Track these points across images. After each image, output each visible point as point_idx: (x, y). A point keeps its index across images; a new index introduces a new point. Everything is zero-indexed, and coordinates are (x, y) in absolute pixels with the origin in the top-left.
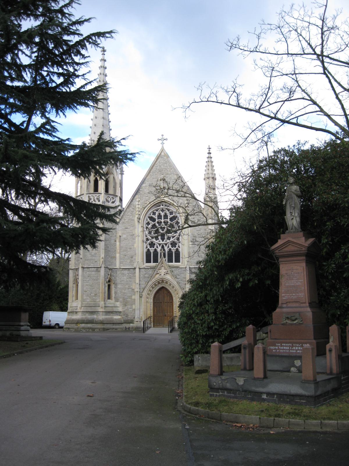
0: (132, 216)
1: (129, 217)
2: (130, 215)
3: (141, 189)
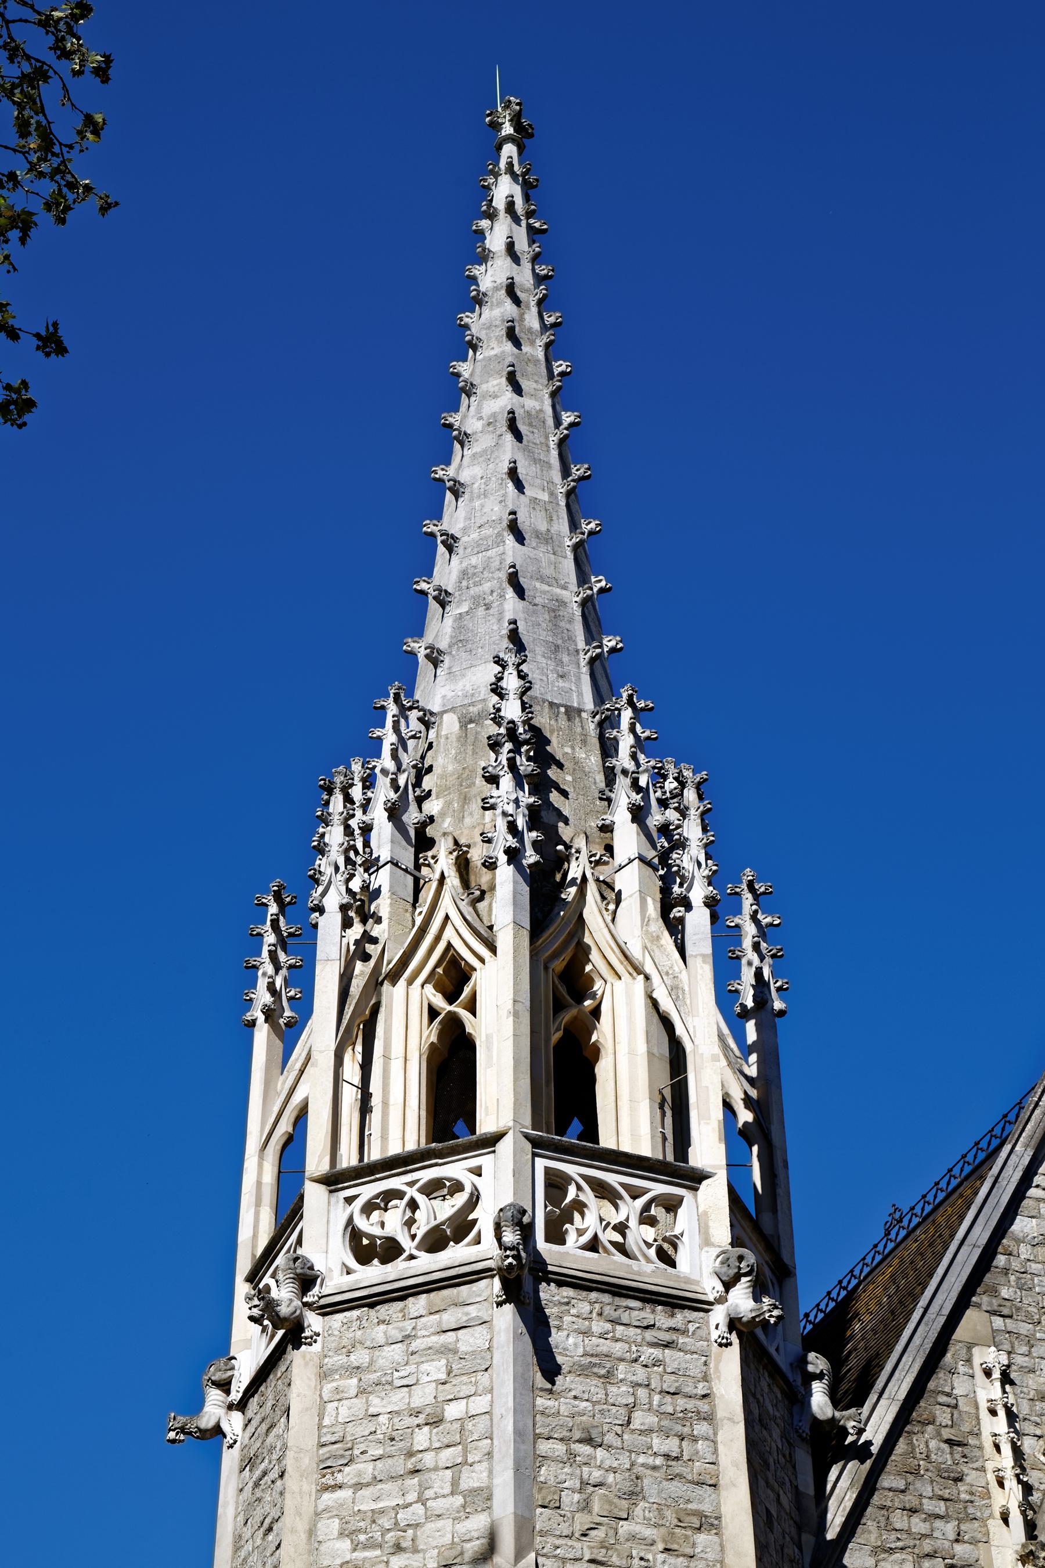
0: (949, 1529)
1: (918, 1525)
2: (929, 1506)
3: (1001, 1260)
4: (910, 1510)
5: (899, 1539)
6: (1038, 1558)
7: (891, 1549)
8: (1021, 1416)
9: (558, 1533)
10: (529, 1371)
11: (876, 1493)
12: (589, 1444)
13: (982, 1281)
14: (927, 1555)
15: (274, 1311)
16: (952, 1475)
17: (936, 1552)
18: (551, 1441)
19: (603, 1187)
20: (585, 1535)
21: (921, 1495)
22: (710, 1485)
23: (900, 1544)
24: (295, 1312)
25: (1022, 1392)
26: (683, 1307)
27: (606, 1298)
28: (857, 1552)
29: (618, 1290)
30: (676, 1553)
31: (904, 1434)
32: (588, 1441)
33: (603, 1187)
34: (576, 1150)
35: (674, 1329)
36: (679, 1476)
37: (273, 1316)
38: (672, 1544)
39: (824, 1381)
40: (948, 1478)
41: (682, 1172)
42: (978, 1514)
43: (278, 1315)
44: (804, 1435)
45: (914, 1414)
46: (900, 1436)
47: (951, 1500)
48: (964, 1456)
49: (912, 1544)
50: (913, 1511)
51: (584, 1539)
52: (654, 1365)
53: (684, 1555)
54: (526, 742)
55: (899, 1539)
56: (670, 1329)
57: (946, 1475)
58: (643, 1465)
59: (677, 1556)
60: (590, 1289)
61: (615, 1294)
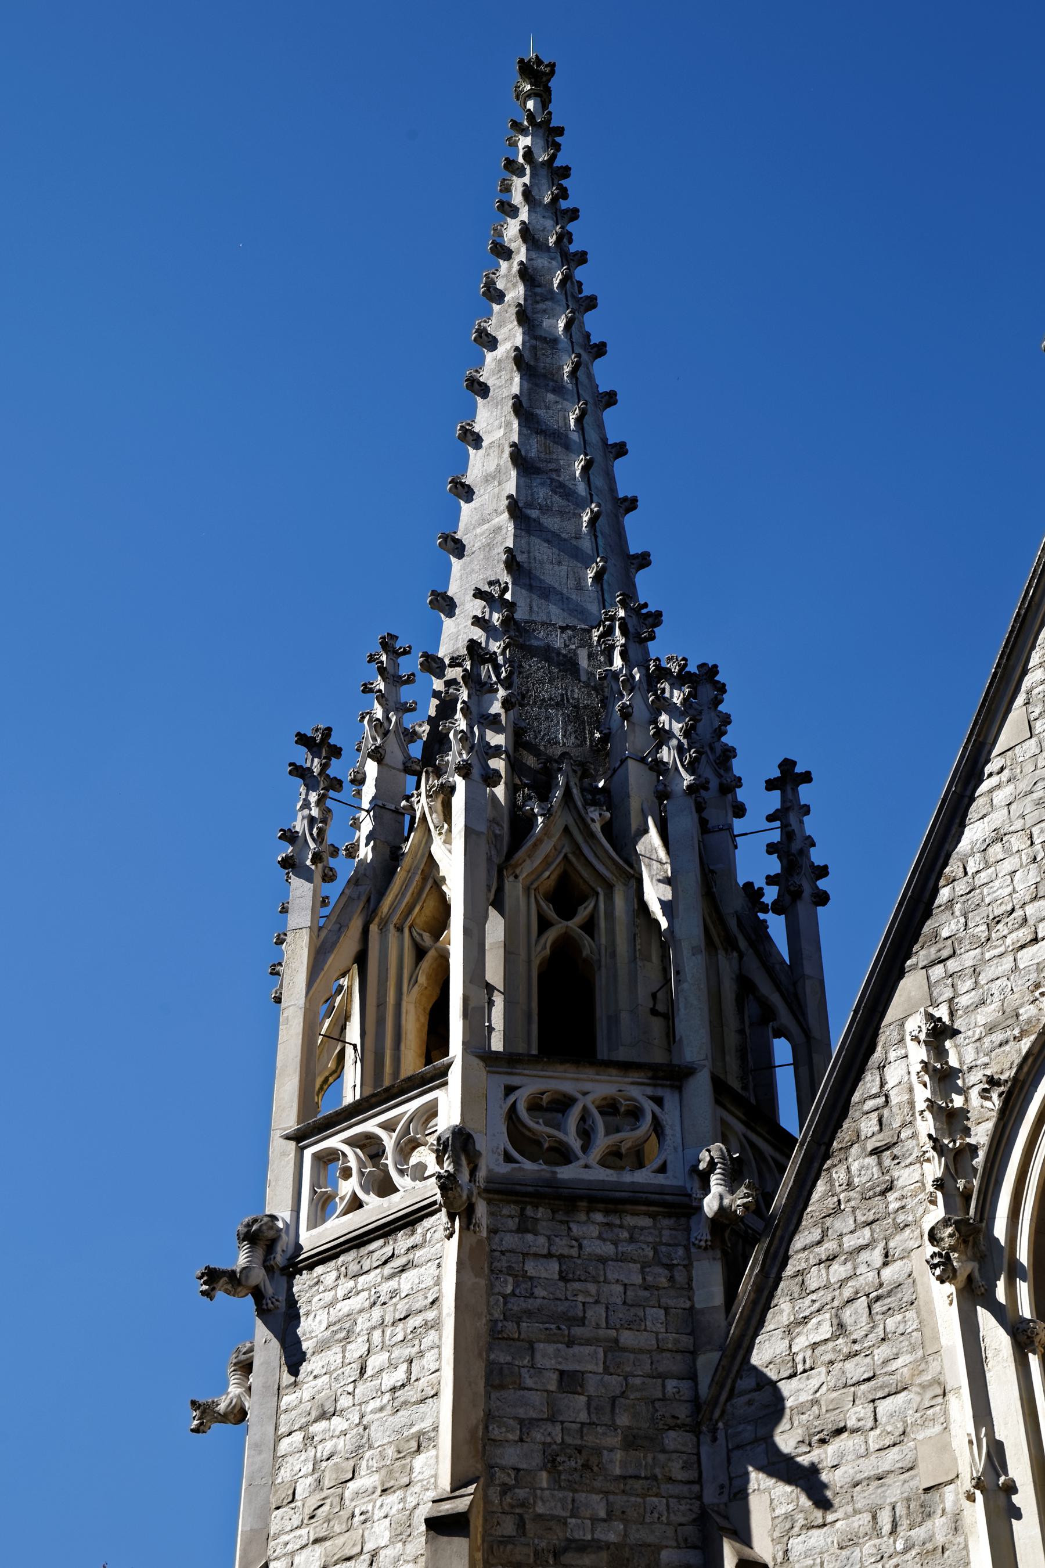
4: (827, 1260)
5: (813, 1301)
6: (942, 1239)
7: (805, 1318)
8: (965, 1068)
9: (289, 1528)
10: (274, 1375)
11: (790, 1262)
12: (323, 1419)
13: (920, 934)
14: (848, 1302)
15: (215, 1412)
16: (878, 1189)
17: (857, 1293)
18: (293, 1434)
19: (370, 1138)
20: (312, 1517)
21: (841, 1235)
22: (432, 1397)
23: (817, 1306)
24: (231, 1402)
25: (965, 1039)
26: (421, 1219)
27: (352, 1255)
28: (767, 1342)
29: (358, 1241)
30: (392, 1490)
31: (823, 1173)
32: (324, 1416)
33: (370, 1138)
34: (334, 1119)
35: (413, 1247)
36: (405, 1403)
37: (216, 1418)
38: (389, 1482)
39: (718, 1171)
40: (875, 1196)
41: (428, 1075)
42: (910, 1218)
43: (220, 1414)
44: (703, 1243)
45: (835, 1144)
46: (817, 1178)
47: (878, 1220)
48: (895, 1158)
49: (829, 1298)
50: (831, 1259)
51: (313, 1521)
52: (391, 1298)
53: (400, 1488)
54: (495, 683)
55: (813, 1301)
56: (408, 1250)
57: (871, 1193)
58: (372, 1412)
59: (394, 1492)
60: (336, 1256)
61: (358, 1246)
